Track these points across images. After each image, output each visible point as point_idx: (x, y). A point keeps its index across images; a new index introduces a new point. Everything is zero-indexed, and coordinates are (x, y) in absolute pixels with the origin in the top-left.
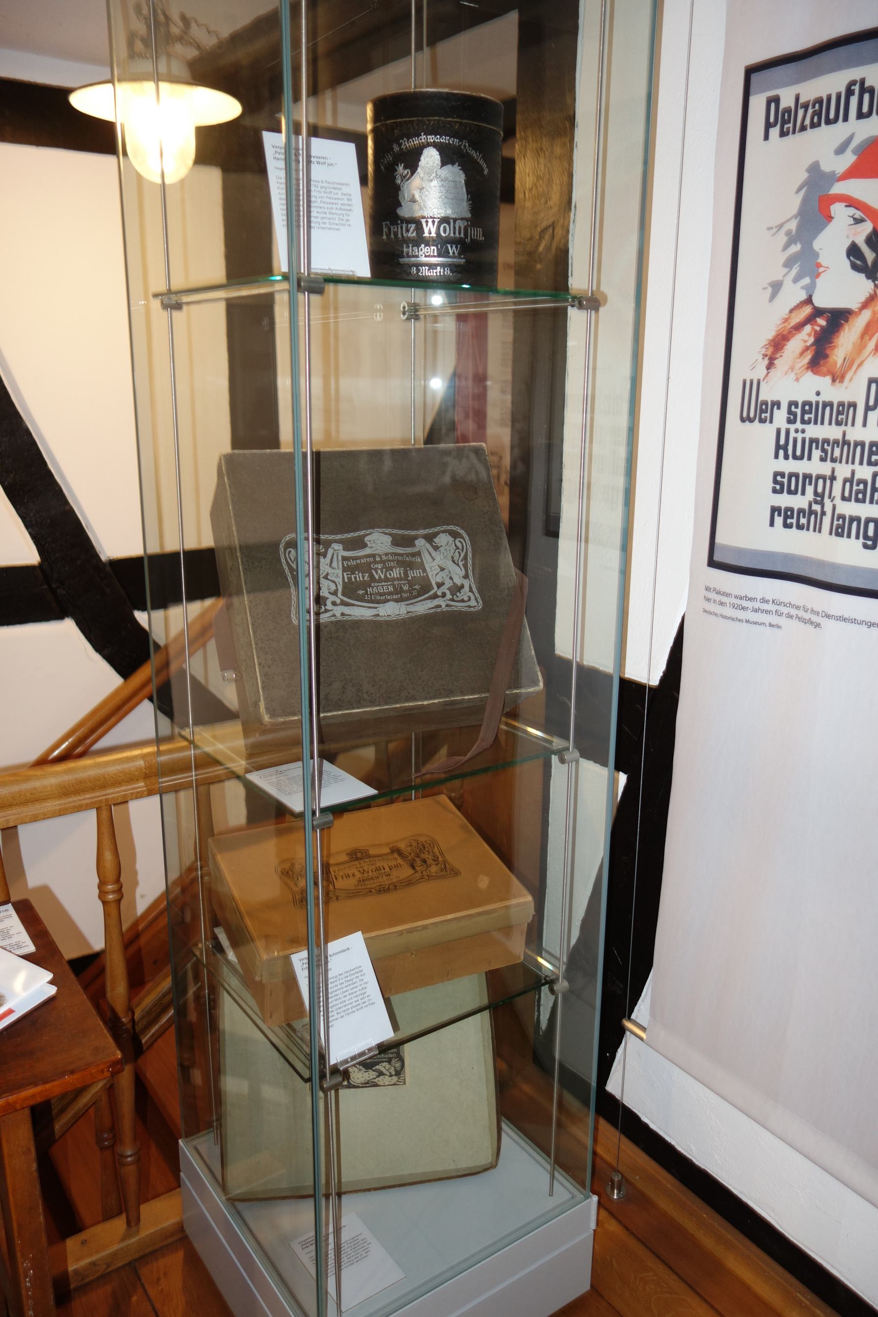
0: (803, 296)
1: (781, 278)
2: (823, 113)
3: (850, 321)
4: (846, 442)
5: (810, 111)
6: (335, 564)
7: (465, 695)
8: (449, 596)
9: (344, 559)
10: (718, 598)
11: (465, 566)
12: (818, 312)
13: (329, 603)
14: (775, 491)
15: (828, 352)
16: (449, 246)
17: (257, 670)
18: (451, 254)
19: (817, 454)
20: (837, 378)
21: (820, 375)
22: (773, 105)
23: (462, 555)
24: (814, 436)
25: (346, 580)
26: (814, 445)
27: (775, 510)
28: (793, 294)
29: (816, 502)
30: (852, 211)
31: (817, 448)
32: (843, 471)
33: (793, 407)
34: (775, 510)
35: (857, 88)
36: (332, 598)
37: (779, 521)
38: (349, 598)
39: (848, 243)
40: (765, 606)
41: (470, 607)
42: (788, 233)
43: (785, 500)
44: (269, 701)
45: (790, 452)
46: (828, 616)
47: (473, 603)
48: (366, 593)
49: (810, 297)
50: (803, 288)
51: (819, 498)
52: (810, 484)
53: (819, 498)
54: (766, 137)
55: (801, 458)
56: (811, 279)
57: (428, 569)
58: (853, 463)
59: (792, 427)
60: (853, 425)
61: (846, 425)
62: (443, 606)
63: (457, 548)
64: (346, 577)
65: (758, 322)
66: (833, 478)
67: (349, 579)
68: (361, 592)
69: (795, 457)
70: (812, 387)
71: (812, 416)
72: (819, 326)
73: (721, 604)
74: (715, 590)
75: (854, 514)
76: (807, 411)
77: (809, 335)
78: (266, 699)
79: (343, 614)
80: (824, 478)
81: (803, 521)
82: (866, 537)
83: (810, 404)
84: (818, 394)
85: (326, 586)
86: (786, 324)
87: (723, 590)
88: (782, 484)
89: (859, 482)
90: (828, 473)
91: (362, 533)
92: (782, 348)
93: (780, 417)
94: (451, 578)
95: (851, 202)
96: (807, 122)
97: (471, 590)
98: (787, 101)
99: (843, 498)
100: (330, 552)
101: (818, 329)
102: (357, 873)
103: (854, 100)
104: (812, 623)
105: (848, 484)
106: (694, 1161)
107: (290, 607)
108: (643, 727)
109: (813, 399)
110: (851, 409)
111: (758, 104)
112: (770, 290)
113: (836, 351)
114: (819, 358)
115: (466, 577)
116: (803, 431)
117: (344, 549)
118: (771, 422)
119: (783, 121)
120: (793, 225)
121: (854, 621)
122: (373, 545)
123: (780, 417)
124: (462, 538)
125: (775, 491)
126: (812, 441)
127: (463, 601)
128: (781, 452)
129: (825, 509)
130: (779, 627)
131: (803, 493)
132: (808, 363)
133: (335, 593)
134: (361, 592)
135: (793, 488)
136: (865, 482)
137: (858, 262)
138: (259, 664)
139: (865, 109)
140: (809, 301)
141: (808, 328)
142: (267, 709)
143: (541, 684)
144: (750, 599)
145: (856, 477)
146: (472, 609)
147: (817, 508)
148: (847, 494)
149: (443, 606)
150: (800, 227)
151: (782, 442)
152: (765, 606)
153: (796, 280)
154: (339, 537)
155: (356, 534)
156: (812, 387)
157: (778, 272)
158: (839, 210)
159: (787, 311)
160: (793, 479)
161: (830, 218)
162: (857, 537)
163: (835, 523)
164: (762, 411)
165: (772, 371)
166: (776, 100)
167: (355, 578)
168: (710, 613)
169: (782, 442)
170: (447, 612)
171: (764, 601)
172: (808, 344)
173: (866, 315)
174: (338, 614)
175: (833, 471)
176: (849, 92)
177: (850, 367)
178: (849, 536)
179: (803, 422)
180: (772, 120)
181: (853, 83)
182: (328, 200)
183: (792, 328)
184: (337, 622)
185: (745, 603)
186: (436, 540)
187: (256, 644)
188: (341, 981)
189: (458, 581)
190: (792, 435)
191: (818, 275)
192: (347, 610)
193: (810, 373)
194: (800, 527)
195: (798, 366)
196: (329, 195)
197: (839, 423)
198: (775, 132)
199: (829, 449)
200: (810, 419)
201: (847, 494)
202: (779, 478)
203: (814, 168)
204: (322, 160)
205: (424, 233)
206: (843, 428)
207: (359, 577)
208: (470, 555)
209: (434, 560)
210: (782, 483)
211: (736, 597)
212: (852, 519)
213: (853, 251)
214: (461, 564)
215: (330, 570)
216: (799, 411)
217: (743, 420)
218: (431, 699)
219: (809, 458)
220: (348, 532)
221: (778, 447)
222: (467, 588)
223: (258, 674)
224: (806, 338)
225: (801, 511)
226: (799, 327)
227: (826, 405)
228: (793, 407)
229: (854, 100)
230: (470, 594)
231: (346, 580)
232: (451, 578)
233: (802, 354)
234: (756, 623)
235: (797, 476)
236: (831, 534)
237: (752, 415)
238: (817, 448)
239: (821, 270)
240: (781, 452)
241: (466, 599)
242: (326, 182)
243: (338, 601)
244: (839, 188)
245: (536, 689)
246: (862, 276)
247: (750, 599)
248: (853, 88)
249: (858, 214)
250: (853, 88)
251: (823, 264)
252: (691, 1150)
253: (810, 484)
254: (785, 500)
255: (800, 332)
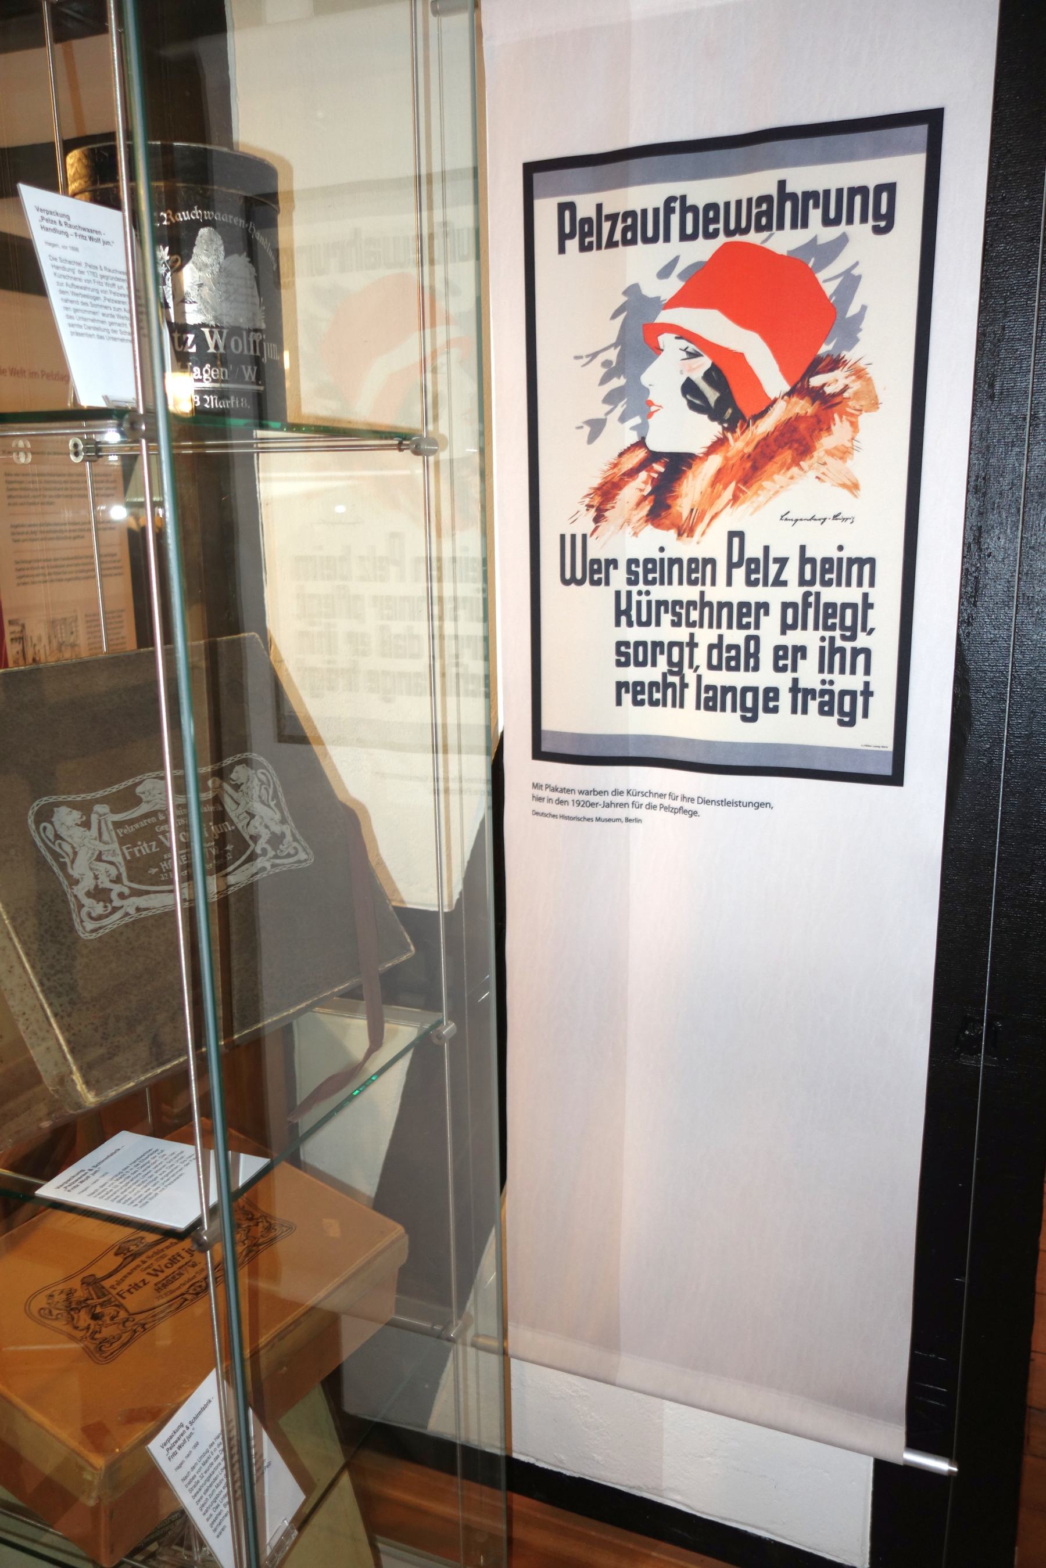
0: (634, 438)
1: (603, 417)
2: (634, 229)
3: (694, 467)
4: (704, 604)
5: (620, 226)
6: (106, 837)
7: (335, 986)
8: (271, 853)
9: (117, 825)
10: (555, 796)
11: (278, 805)
12: (654, 457)
13: (114, 895)
14: (619, 664)
15: (669, 502)
16: (244, 367)
17: (55, 1026)
18: (247, 379)
19: (666, 618)
20: (685, 530)
21: (663, 529)
22: (567, 214)
23: (271, 791)
24: (662, 598)
25: (129, 858)
26: (662, 608)
27: (621, 686)
28: (621, 434)
29: (672, 673)
30: (684, 344)
31: (666, 612)
32: (706, 636)
33: (633, 566)
34: (621, 686)
35: (677, 205)
36: (117, 888)
37: (627, 698)
38: (140, 882)
39: (683, 379)
40: (619, 799)
41: (299, 862)
42: (606, 364)
43: (632, 674)
44: (86, 1071)
45: (634, 618)
46: (707, 802)
47: (302, 856)
48: (161, 871)
49: (643, 439)
50: (633, 428)
51: (675, 668)
52: (662, 653)
53: (675, 668)
54: (562, 250)
55: (648, 624)
56: (643, 419)
57: (235, 820)
58: (719, 626)
59: (634, 589)
60: (713, 583)
61: (704, 584)
62: (269, 867)
63: (262, 783)
64: (126, 852)
65: (574, 468)
66: (692, 644)
67: (132, 854)
68: (154, 871)
69: (640, 624)
70: (650, 542)
71: (657, 575)
72: (656, 472)
73: (560, 802)
74: (548, 786)
75: (728, 683)
76: (655, 570)
77: (645, 483)
78: (80, 1069)
79: (138, 909)
80: (680, 645)
81: (657, 696)
82: (744, 708)
83: (653, 561)
84: (662, 549)
85: (103, 871)
86: (616, 470)
87: (561, 785)
88: (627, 655)
89: (730, 647)
90: (686, 639)
91: (130, 782)
92: (613, 497)
93: (619, 578)
94: (267, 827)
95: (683, 334)
96: (618, 236)
97: (295, 839)
98: (585, 208)
99: (711, 667)
100: (94, 818)
101: (655, 475)
102: (148, 1278)
103: (675, 219)
104: (685, 812)
105: (715, 652)
106: (564, 1472)
107: (70, 913)
108: (459, 967)
109: (657, 555)
110: (709, 568)
111: (546, 210)
112: (587, 429)
113: (679, 501)
114: (659, 508)
115: (283, 821)
116: (648, 593)
117: (113, 811)
118: (607, 583)
119: (582, 233)
120: (612, 355)
121: (739, 804)
122: (149, 798)
123: (619, 578)
124: (264, 767)
125: (619, 664)
126: (659, 603)
127: (289, 856)
128: (624, 619)
129: (686, 681)
130: (638, 821)
131: (654, 664)
132: (647, 515)
133: (118, 880)
134: (154, 871)
135: (641, 659)
136: (737, 647)
137: (697, 402)
138: (56, 1015)
139: (689, 230)
140: (641, 443)
141: (643, 475)
142: (87, 1083)
143: (412, 948)
144: (600, 793)
145: (726, 643)
146: (304, 865)
147: (675, 679)
148: (715, 662)
149: (269, 867)
150: (621, 356)
151: (623, 606)
152: (619, 799)
153: (623, 419)
154: (100, 794)
155: (123, 785)
156: (650, 542)
157: (599, 411)
158: (666, 340)
159: (616, 454)
160: (641, 649)
161: (659, 351)
162: (734, 710)
163: (703, 696)
164: (593, 572)
165: (603, 525)
166: (571, 207)
167: (140, 851)
168: (543, 815)
169: (623, 606)
170: (276, 874)
171: (617, 793)
172: (646, 493)
173: (715, 462)
174: (132, 911)
175: (692, 635)
176: (669, 210)
177: (701, 518)
178: (723, 709)
179: (647, 582)
180: (567, 230)
181: (671, 199)
182: (112, 297)
183: (624, 474)
184: (133, 923)
185: (592, 798)
186: (233, 776)
187: (41, 984)
188: (215, 1455)
189: (277, 829)
190: (635, 598)
191: (650, 415)
192: (142, 902)
193: (650, 527)
194: (654, 703)
195: (635, 519)
196: (114, 290)
197: (693, 583)
198: (572, 245)
199: (683, 612)
200: (654, 579)
201: (715, 662)
202: (623, 649)
203: (633, 291)
204: (95, 236)
205: (208, 348)
206: (699, 588)
207: (144, 848)
208: (280, 789)
209: (238, 804)
210: (624, 653)
211: (581, 792)
212: (725, 690)
213: (689, 388)
214: (272, 804)
215: (102, 847)
216: (640, 570)
217: (566, 582)
218: (297, 1003)
219: (658, 624)
220: (111, 784)
221: (619, 613)
222: (289, 837)
223: (58, 1032)
224: (642, 486)
225: (653, 684)
226: (633, 473)
227: (672, 562)
228: (633, 566)
229: (675, 219)
230: (295, 844)
231: (129, 858)
232: (267, 827)
233: (638, 504)
234: (609, 820)
235: (644, 644)
236: (698, 707)
237: (579, 575)
238: (666, 612)
239: (653, 408)
240: (624, 619)
241: (292, 852)
242: (106, 268)
243: (127, 891)
244: (665, 317)
245: (408, 955)
246: (704, 418)
247: (600, 793)
248: (672, 205)
249: (692, 348)
250: (672, 205)
251: (655, 402)
252: (561, 1461)
253: (662, 653)
254: (632, 674)
255: (634, 480)
